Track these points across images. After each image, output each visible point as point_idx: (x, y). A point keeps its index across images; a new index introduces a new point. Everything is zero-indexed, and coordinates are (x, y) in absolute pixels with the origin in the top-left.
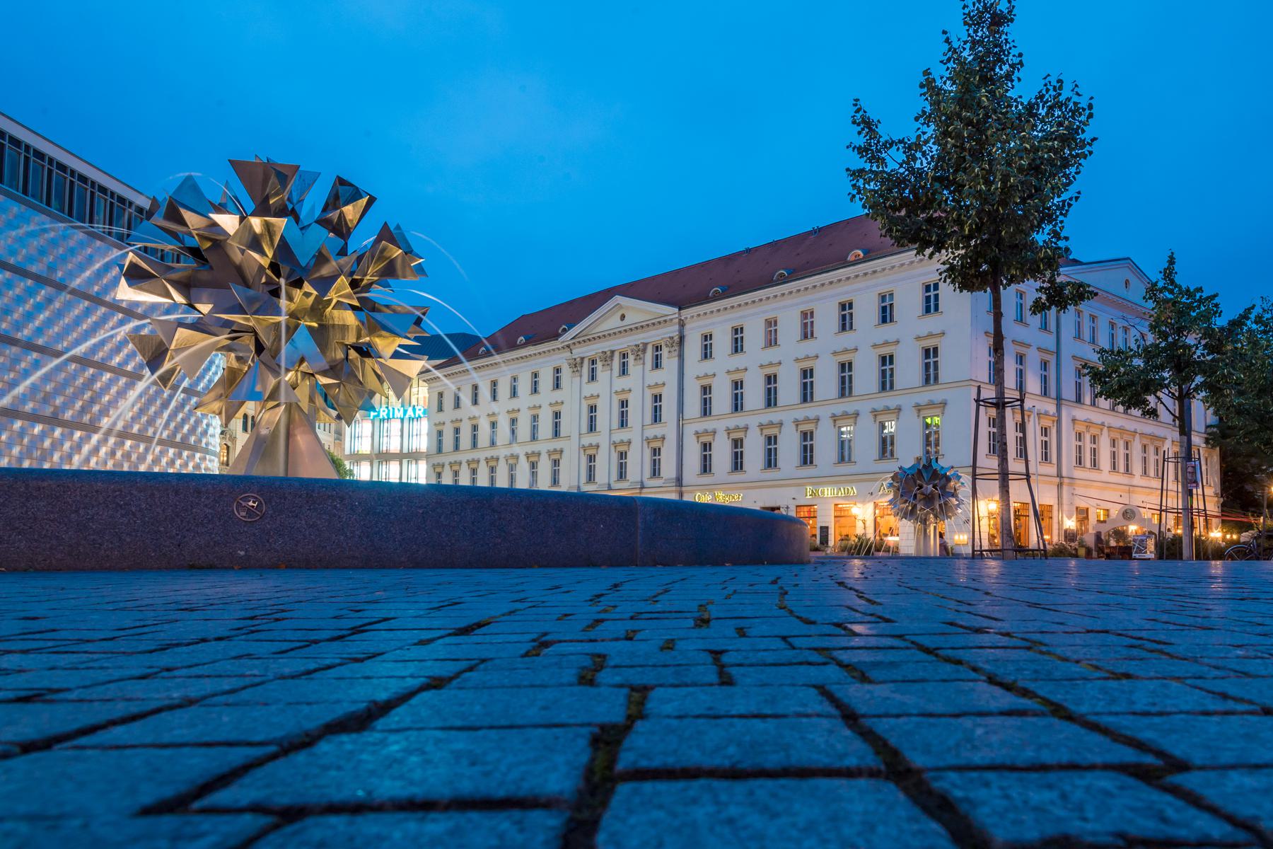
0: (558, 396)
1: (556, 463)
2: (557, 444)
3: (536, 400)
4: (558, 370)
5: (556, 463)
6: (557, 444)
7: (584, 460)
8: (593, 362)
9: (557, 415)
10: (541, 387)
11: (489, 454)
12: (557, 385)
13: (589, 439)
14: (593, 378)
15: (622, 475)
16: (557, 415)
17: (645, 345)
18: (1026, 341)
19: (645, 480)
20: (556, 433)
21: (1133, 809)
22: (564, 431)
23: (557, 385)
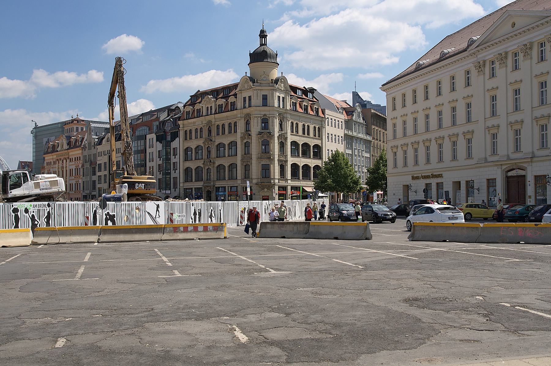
0: (469, 91)
1: (469, 141)
2: (470, 127)
3: (440, 100)
4: (468, 72)
5: (469, 141)
6: (470, 127)
7: (489, 138)
8: (493, 63)
9: (469, 105)
10: (418, 99)
11: (413, 140)
12: (468, 84)
13: (492, 122)
14: (516, 68)
15: (517, 148)
16: (469, 105)
17: (531, 44)
18: (518, 80)
19: (488, 157)
20: (469, 120)
21: (261, 270)
22: (473, 118)
23: (468, 84)
